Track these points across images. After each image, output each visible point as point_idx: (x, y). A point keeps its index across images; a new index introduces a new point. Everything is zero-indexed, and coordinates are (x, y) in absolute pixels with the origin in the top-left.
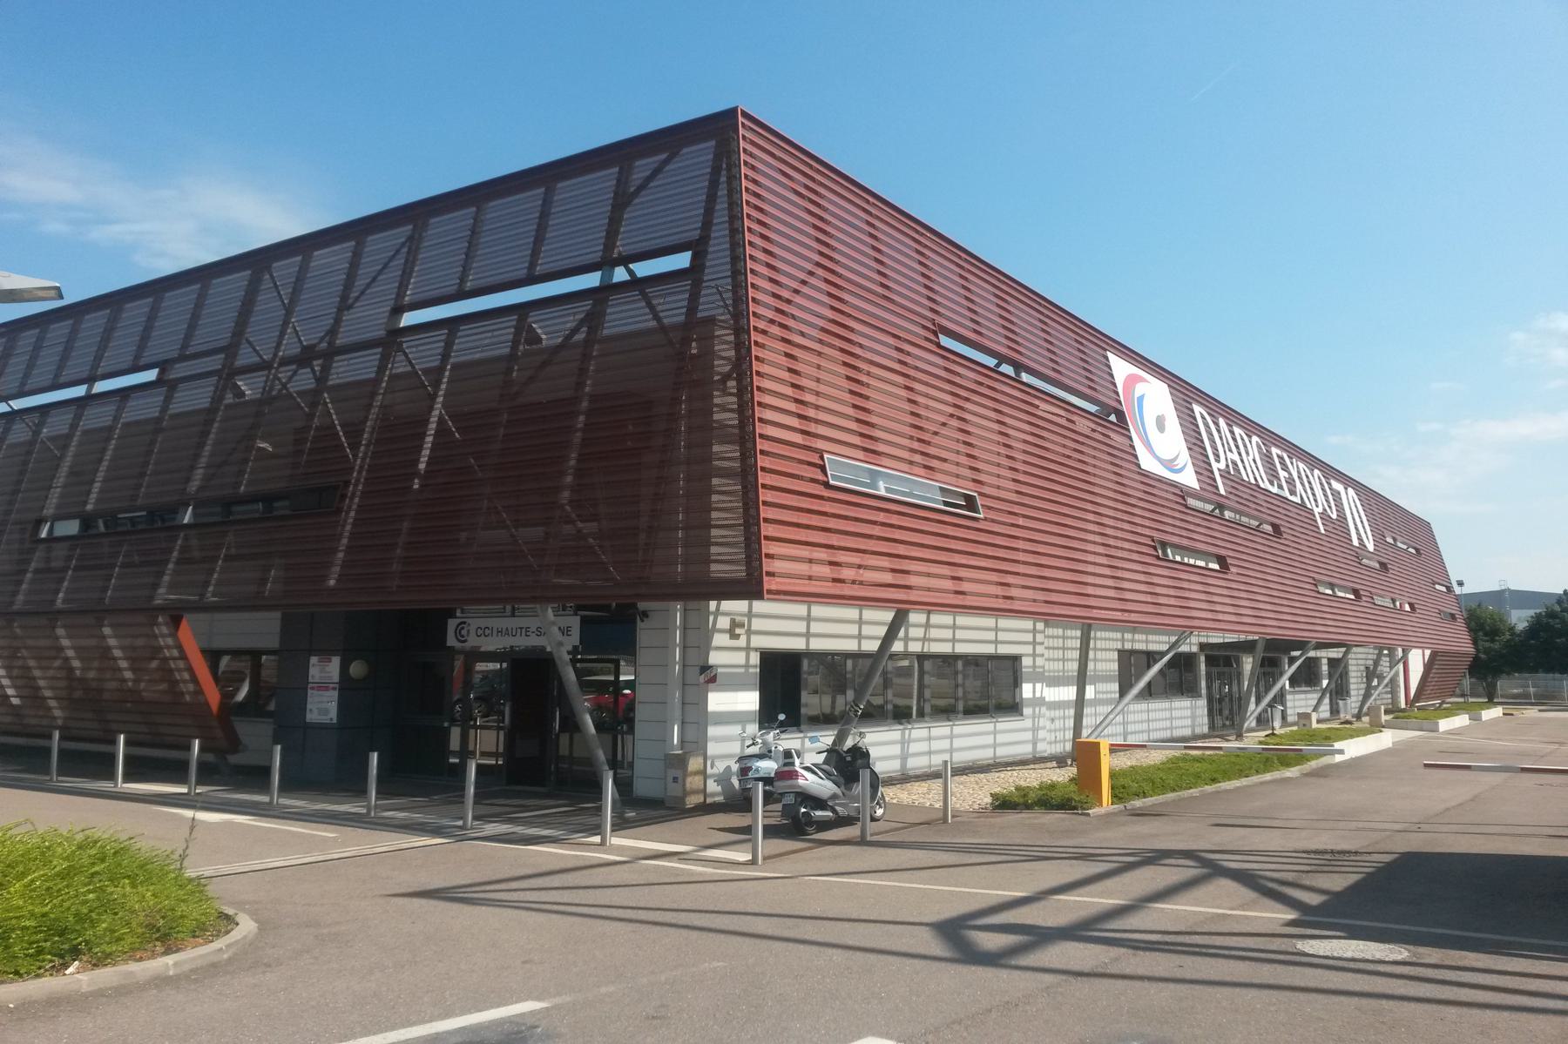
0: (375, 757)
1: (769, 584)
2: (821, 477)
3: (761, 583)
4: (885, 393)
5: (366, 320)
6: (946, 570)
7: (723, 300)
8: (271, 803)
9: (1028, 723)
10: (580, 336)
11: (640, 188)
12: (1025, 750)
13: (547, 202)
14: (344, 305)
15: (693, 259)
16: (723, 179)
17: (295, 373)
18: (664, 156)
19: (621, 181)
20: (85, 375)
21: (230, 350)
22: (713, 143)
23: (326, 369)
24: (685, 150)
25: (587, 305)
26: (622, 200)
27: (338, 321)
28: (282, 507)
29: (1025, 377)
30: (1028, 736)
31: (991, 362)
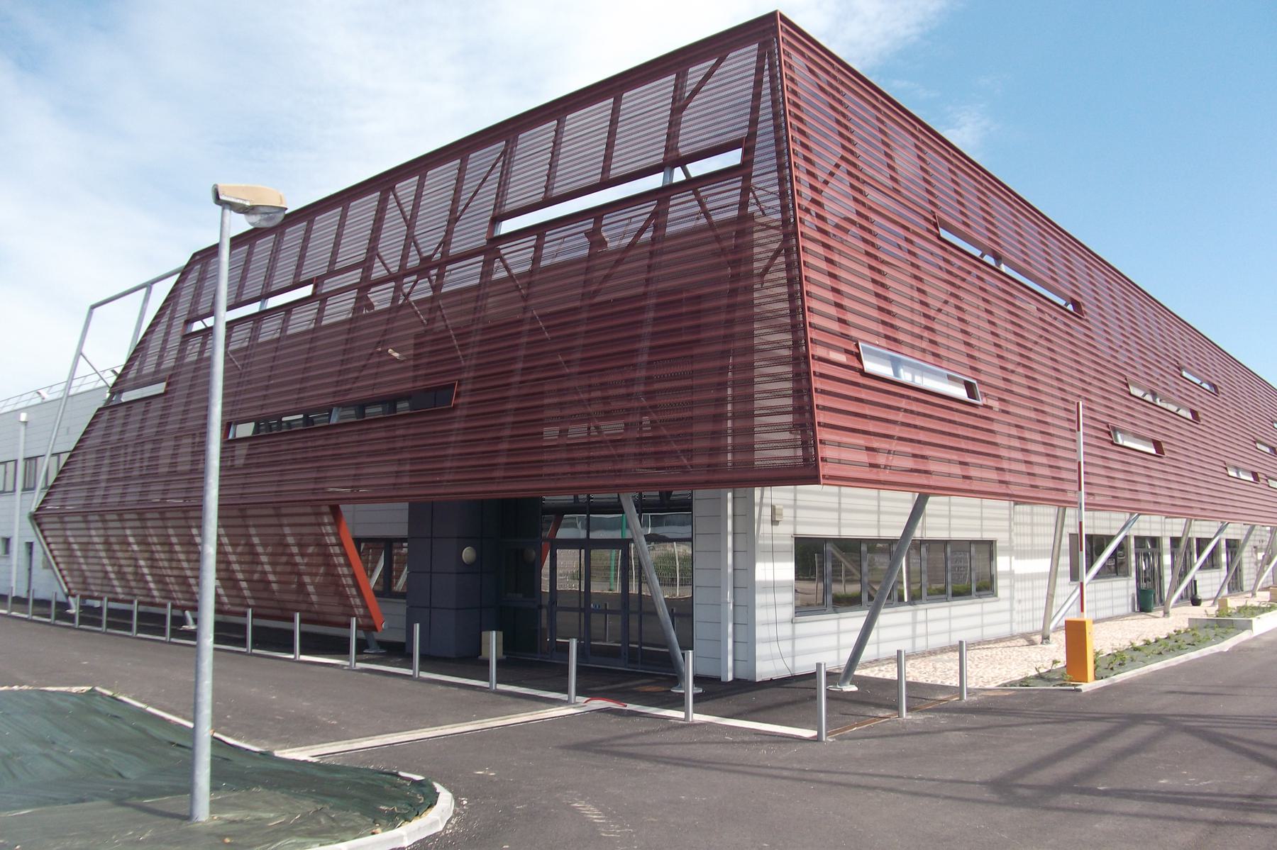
0: (418, 625)
1: (824, 470)
2: (857, 365)
3: (817, 467)
4: (899, 285)
5: (470, 235)
6: (954, 456)
7: (755, 198)
8: (817, 739)
9: (1004, 605)
10: (647, 235)
11: (695, 92)
12: (1004, 630)
13: (616, 111)
14: (453, 219)
15: (744, 154)
16: (766, 79)
17: (416, 282)
18: (713, 61)
19: (678, 87)
20: (258, 293)
21: (366, 265)
22: (756, 46)
23: (440, 276)
24: (731, 55)
25: (650, 207)
26: (679, 106)
27: (449, 232)
28: (403, 406)
29: (1003, 268)
30: (1006, 616)
31: (977, 253)
